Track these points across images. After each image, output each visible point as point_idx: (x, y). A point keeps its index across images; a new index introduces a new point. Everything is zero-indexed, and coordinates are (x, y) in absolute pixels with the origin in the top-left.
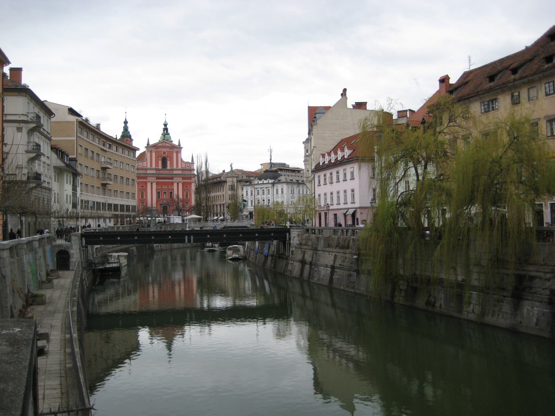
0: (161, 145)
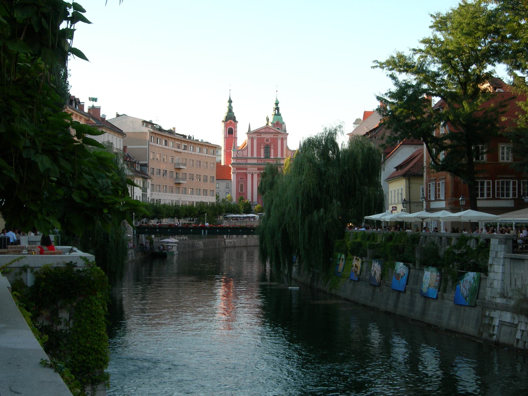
0: (263, 131)
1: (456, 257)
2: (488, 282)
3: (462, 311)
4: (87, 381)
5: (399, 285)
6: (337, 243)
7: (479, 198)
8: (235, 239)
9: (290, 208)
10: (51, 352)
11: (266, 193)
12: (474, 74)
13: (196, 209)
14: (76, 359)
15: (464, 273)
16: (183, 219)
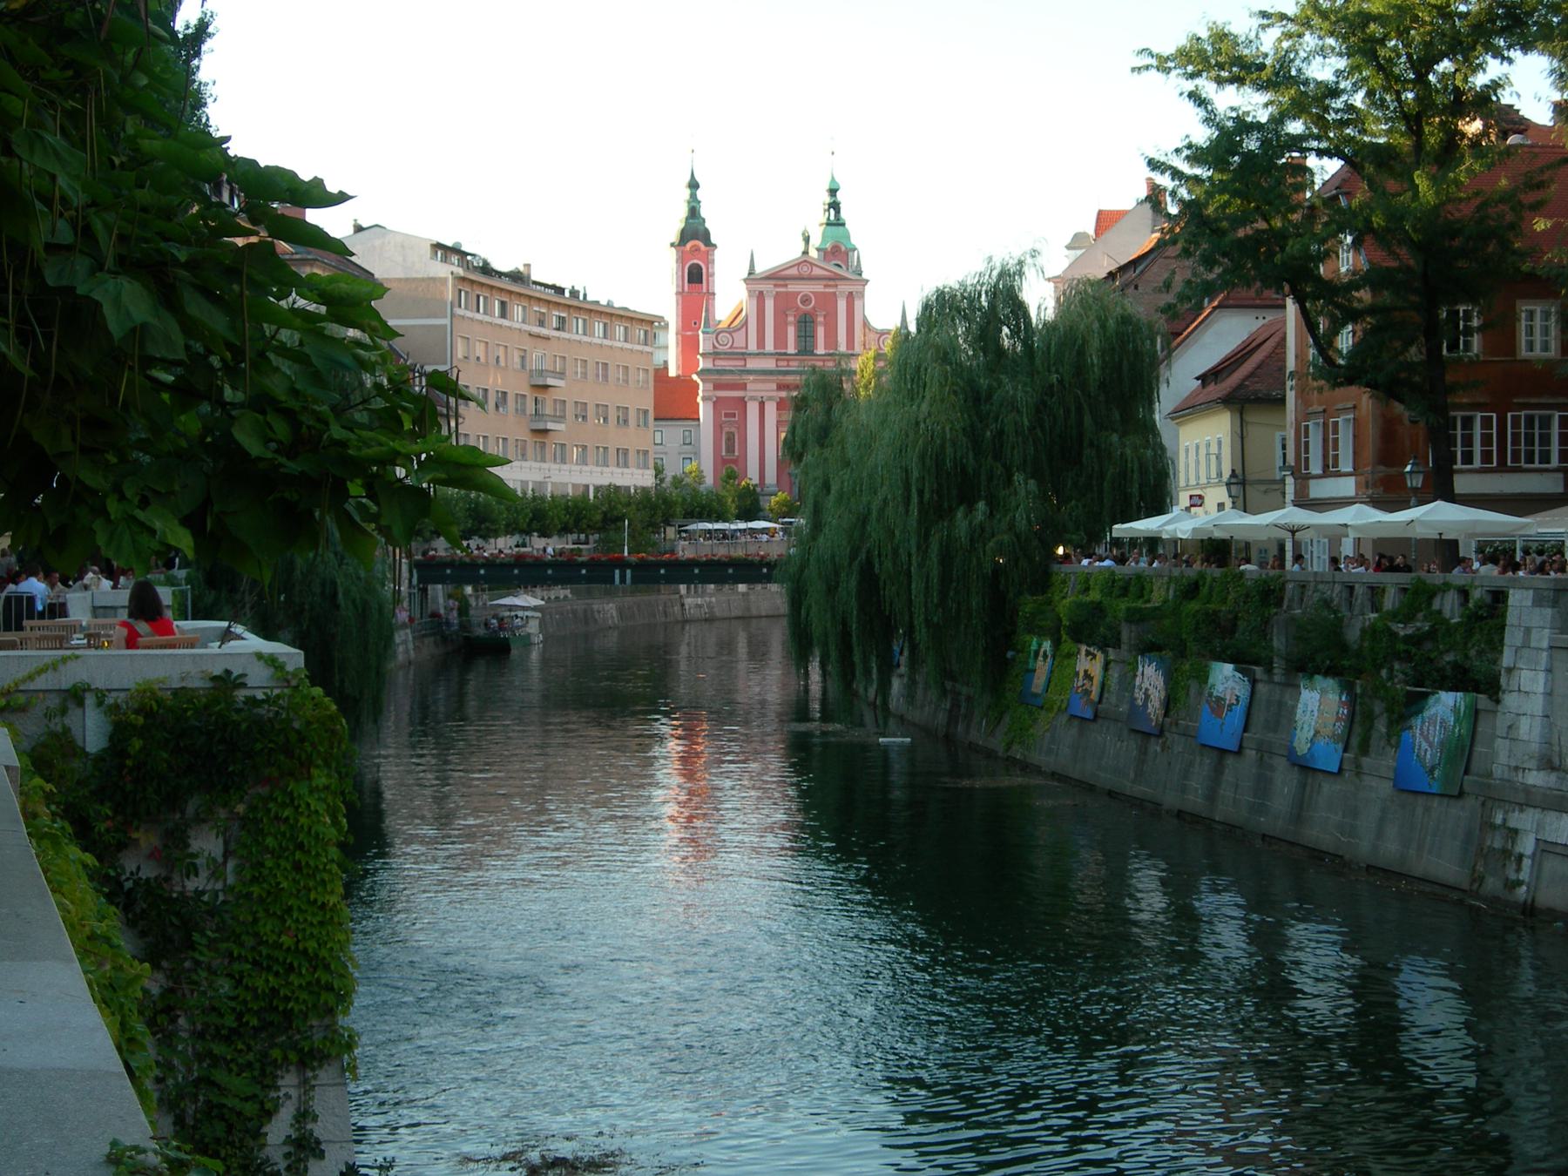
0: (794, 271)
1: (1401, 647)
2: (1501, 723)
3: (1419, 811)
4: (285, 1058)
5: (1225, 730)
6: (1028, 604)
7: (1459, 466)
8: (711, 595)
9: (885, 501)
10: (165, 964)
11: (808, 458)
12: (1446, 88)
13: (595, 507)
14: (247, 988)
15: (1425, 696)
16: (555, 538)
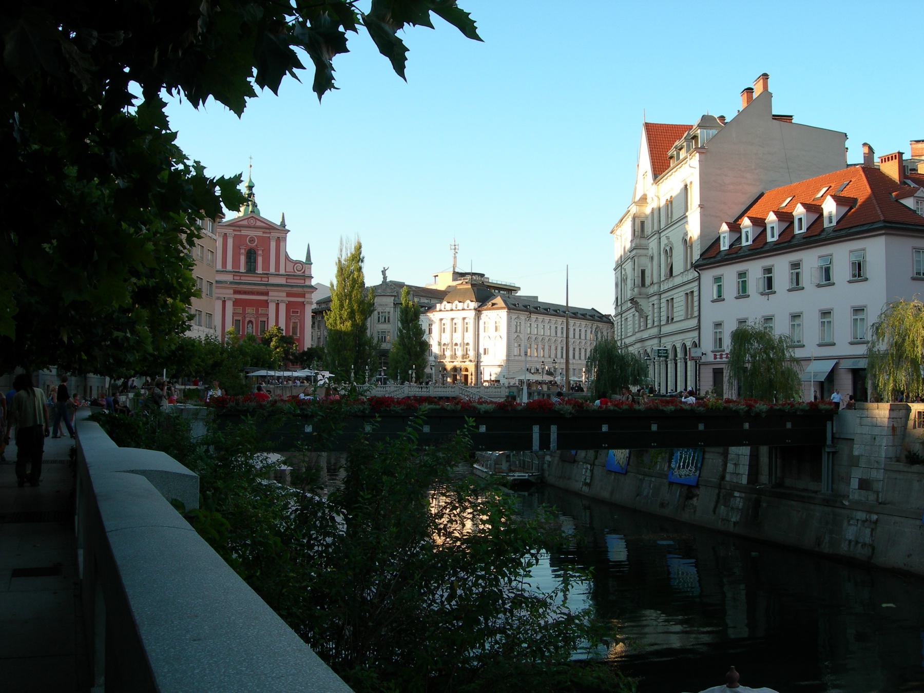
0: (245, 223)
